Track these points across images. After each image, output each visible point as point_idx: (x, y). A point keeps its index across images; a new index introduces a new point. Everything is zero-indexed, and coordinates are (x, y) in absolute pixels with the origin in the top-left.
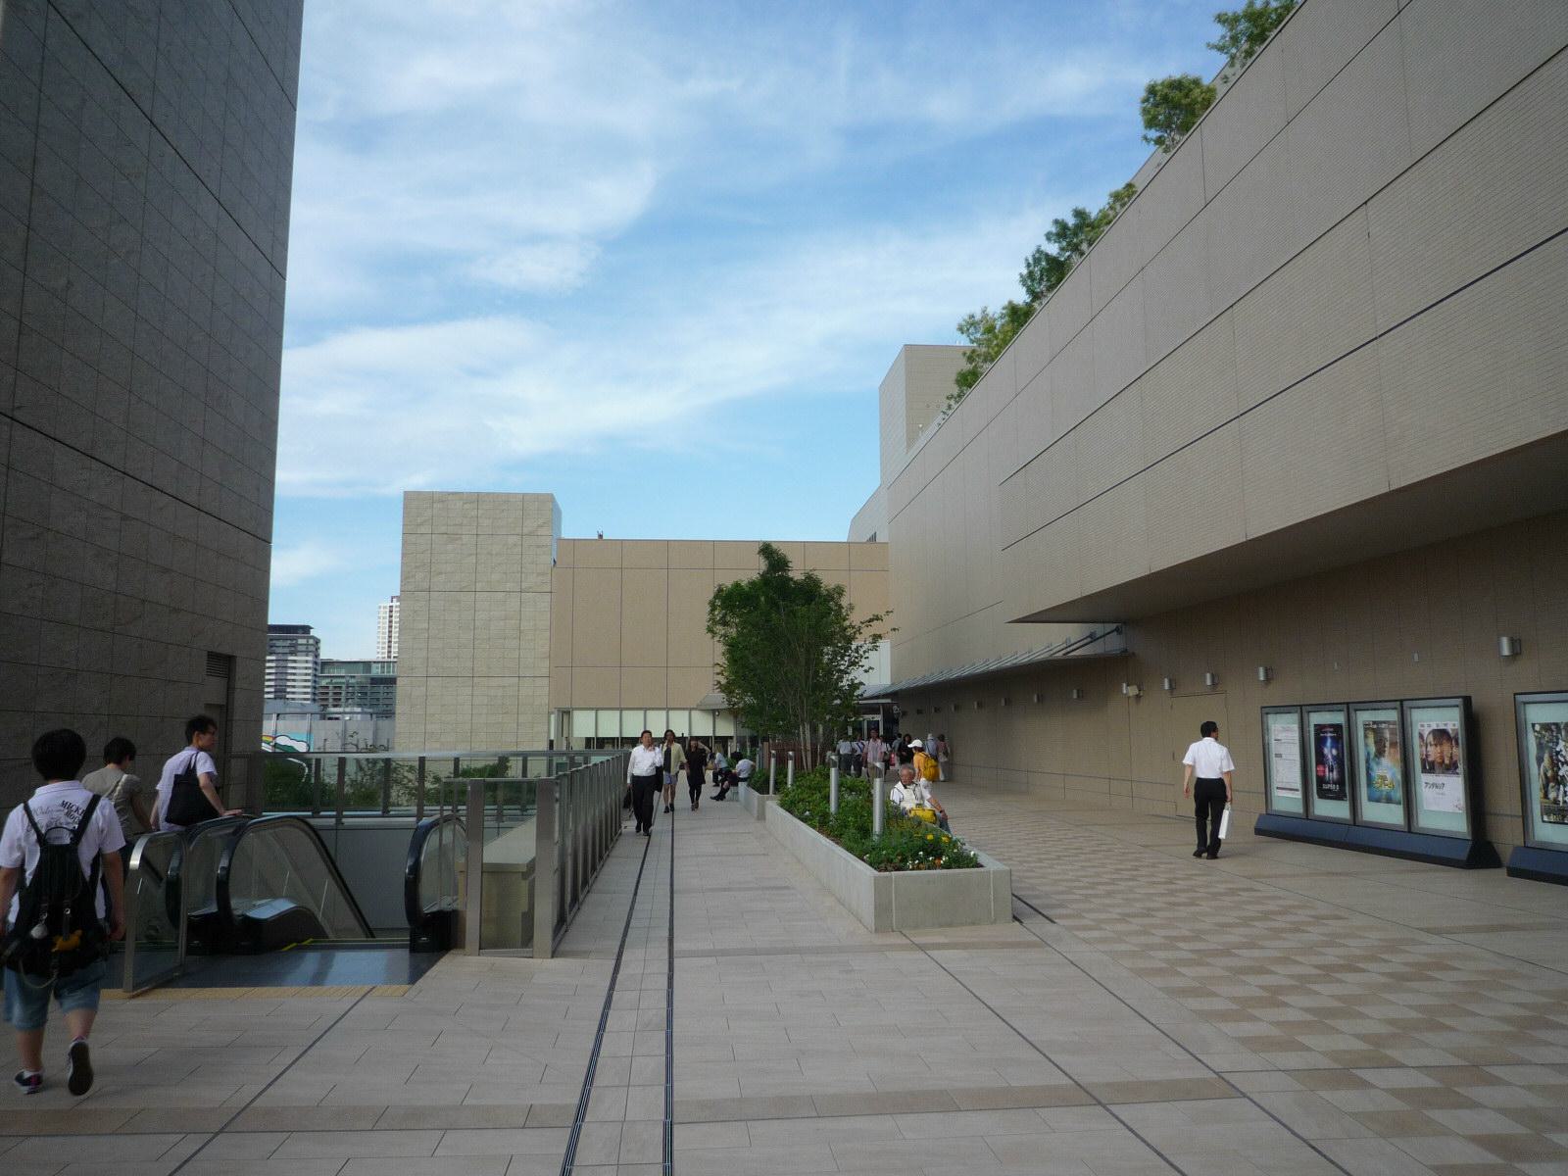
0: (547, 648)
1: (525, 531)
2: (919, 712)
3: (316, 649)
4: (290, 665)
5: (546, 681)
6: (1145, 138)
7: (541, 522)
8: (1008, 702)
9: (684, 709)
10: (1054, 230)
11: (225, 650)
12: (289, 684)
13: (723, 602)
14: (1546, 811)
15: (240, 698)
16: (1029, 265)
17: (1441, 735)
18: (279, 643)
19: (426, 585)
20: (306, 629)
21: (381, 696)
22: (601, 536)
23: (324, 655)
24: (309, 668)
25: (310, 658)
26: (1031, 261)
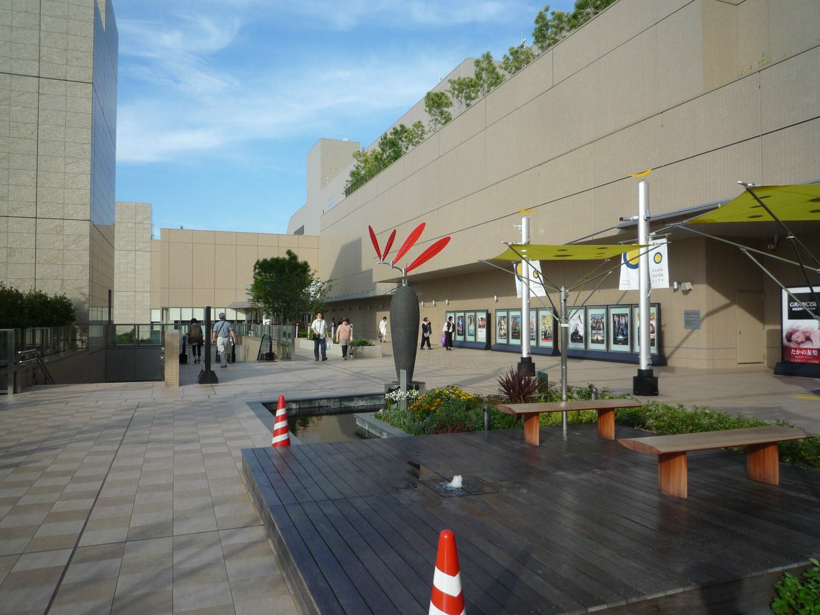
0: (149, 278)
1: (137, 221)
2: (333, 310)
6: (426, 110)
7: (145, 217)
8: (371, 308)
9: (223, 308)
10: (393, 131)
13: (260, 266)
14: (499, 336)
16: (382, 139)
17: (482, 319)
22: (182, 228)
26: (383, 138)
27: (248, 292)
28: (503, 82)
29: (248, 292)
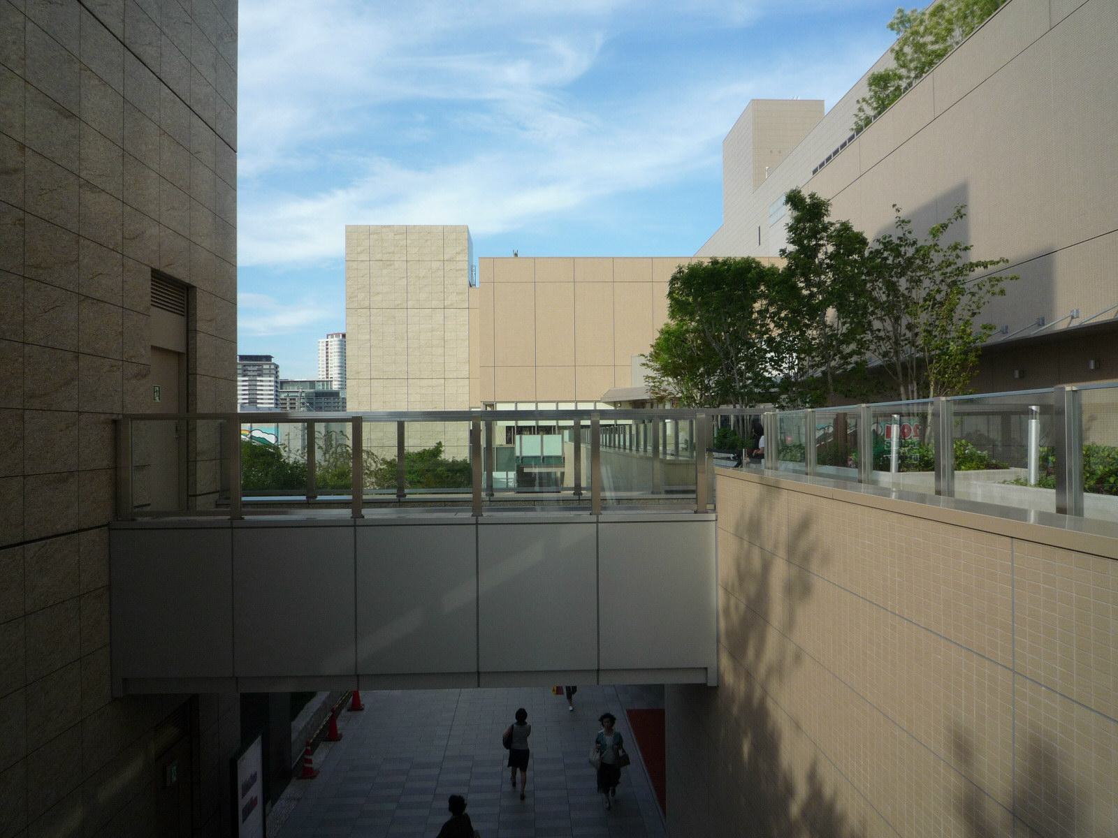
0: (466, 355)
1: (446, 257)
3: (277, 372)
4: (258, 383)
5: (466, 381)
11: (181, 273)
12: (258, 397)
15: (204, 346)
18: (249, 368)
19: (367, 304)
20: (268, 358)
21: (323, 405)
22: (516, 255)
23: (282, 377)
24: (272, 399)
25: (272, 379)
27: (643, 360)
28: (903, 95)
29: (643, 360)
